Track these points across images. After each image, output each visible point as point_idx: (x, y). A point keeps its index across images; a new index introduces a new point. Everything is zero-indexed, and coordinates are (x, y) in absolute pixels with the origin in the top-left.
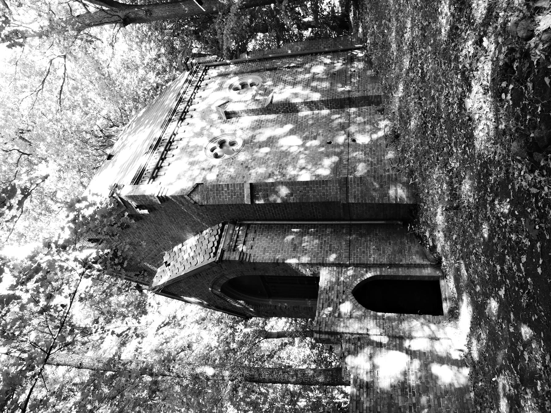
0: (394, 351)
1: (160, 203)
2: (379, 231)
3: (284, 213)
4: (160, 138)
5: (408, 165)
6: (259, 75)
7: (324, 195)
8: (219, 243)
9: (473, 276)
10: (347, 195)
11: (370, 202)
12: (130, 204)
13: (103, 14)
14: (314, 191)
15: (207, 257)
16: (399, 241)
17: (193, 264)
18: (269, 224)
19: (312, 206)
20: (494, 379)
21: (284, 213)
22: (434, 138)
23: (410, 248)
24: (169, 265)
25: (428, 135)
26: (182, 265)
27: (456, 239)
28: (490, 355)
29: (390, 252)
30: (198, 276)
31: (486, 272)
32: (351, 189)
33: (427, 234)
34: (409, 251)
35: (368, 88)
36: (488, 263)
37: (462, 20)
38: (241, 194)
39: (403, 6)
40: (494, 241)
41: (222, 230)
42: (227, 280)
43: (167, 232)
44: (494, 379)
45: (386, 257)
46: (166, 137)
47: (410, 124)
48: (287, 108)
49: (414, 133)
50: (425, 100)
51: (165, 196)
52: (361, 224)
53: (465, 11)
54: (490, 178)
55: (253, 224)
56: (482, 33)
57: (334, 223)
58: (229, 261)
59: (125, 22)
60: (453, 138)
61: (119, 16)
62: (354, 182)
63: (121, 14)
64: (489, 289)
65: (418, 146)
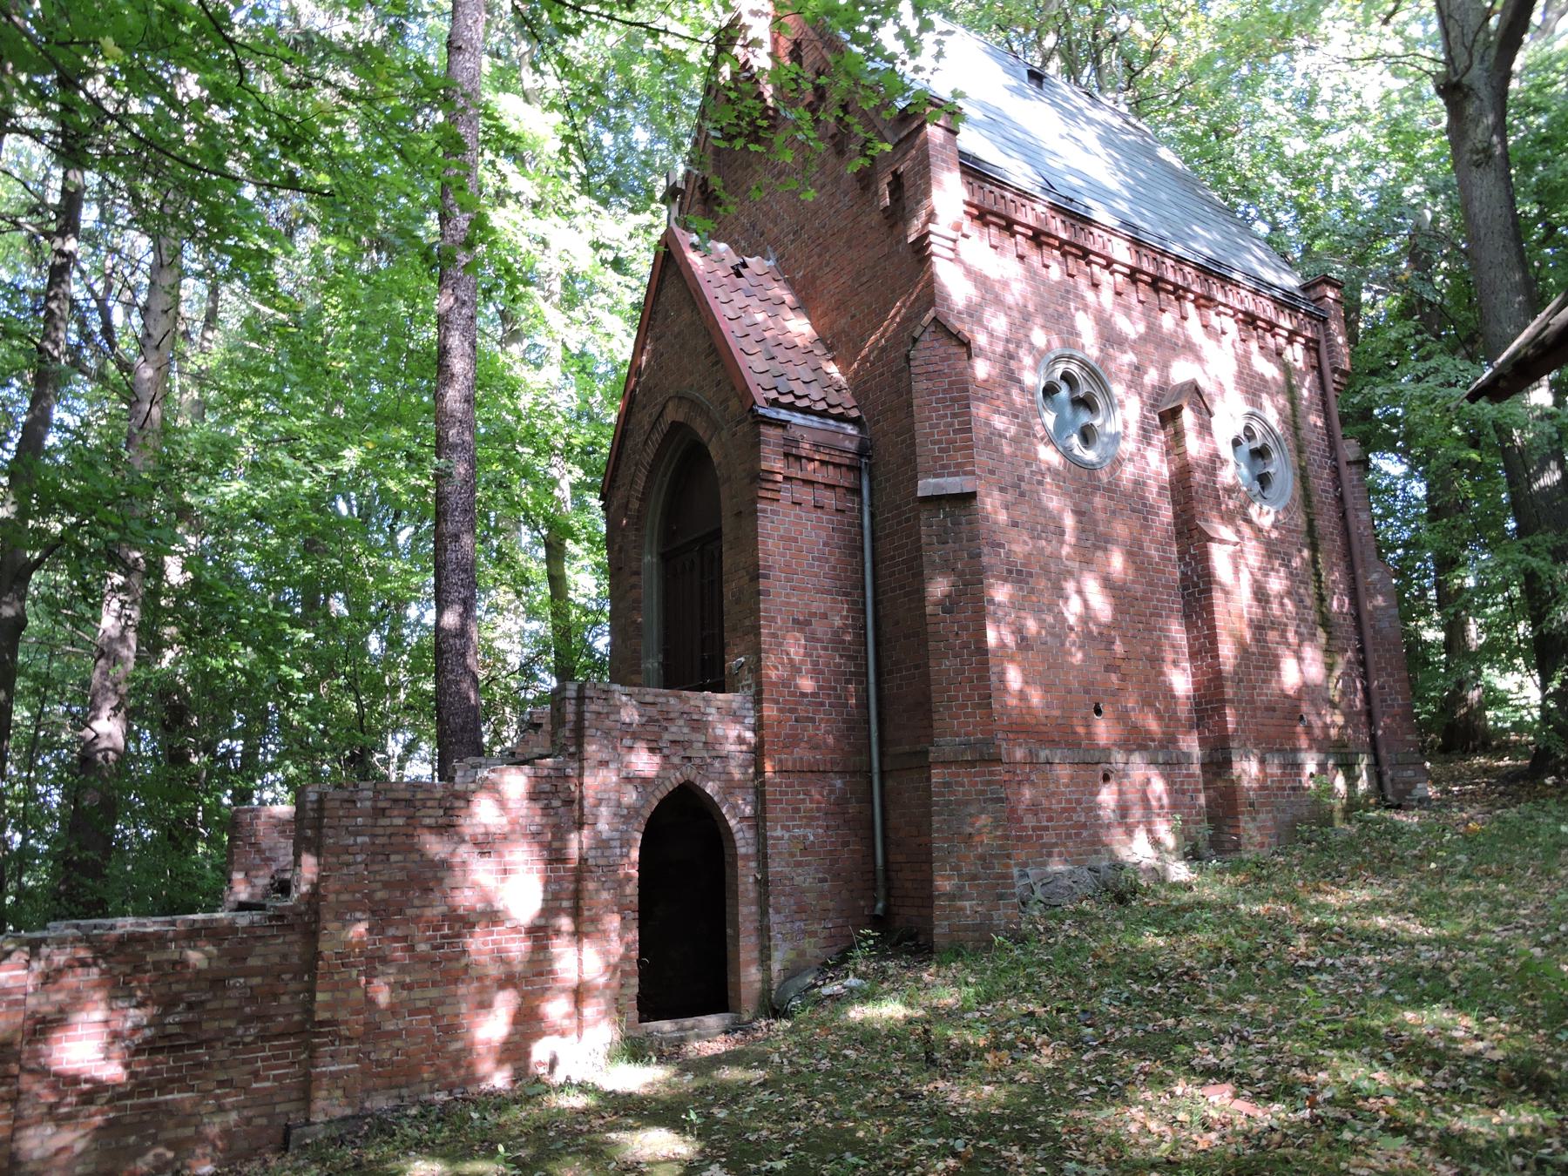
0: (540, 896)
1: (910, 240)
2: (854, 851)
3: (893, 590)
4: (1089, 221)
5: (1041, 928)
6: (1293, 499)
7: (950, 699)
8: (806, 411)
9: (752, 1100)
10: (951, 763)
11: (935, 826)
12: (905, 154)
13: (1474, 20)
14: (960, 672)
15: (766, 381)
16: (831, 905)
17: (744, 343)
18: (862, 549)
19: (917, 667)
20: (501, 1148)
21: (893, 590)
22: (1119, 1000)
23: (813, 934)
24: (739, 275)
25: (1128, 986)
26: (740, 313)
27: (846, 1057)
28: (553, 1140)
29: (798, 880)
30: (713, 358)
31: (764, 1133)
32: (968, 775)
33: (852, 981)
34: (804, 932)
35: (1262, 816)
36: (790, 1140)
37: (1461, 1080)
38: (944, 467)
39: (1510, 916)
40: (848, 1154)
41: (840, 418)
42: (705, 439)
43: (828, 264)
44: (501, 1148)
45: (787, 870)
46: (1096, 241)
47: (1157, 935)
48: (1196, 585)
49: (1132, 946)
50: (1229, 977)
51: (932, 254)
52: (872, 802)
53: (1486, 1090)
54: (1015, 1149)
55: (861, 503)
56: (1419, 1134)
57: (874, 727)
58: (759, 443)
59: (1452, 90)
60: (1120, 1052)
61: (1468, 68)
62: (989, 783)
63: (1477, 76)
64: (721, 1141)
65: (1096, 956)
